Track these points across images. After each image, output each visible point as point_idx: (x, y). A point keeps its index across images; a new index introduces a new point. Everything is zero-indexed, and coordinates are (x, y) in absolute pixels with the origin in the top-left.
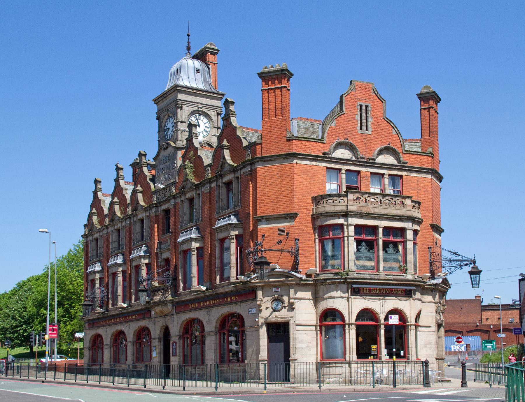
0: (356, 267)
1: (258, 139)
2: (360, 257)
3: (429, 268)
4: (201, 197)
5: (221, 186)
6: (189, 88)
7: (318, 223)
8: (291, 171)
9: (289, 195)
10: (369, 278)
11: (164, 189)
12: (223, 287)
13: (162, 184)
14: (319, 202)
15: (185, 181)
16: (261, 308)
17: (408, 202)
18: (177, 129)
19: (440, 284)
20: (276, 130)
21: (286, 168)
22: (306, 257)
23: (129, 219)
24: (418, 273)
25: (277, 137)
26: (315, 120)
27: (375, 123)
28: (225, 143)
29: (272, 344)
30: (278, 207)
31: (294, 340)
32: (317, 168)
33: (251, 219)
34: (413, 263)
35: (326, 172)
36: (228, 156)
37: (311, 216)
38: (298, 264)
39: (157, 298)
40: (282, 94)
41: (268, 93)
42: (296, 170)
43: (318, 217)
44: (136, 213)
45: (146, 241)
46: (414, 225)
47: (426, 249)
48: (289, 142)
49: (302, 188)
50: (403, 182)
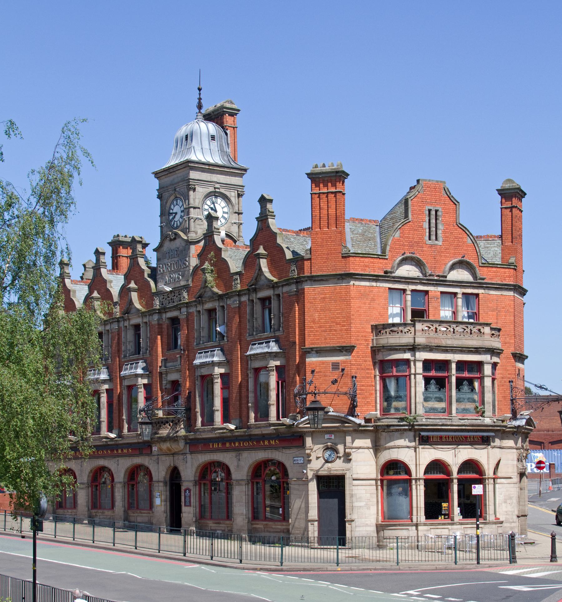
0: (424, 411)
1: (307, 254)
2: (429, 397)
3: (510, 407)
4: (225, 311)
5: (255, 302)
6: (203, 164)
7: (380, 357)
8: (347, 294)
9: (344, 323)
10: (440, 423)
11: (171, 291)
12: (259, 427)
13: (166, 284)
14: (380, 332)
15: (204, 288)
16: (310, 458)
17: (487, 330)
18: (189, 218)
19: (523, 426)
20: (328, 244)
21: (341, 291)
22: (365, 398)
23: (117, 323)
24: (496, 414)
25: (329, 252)
26: (370, 221)
27: (446, 231)
28: (261, 250)
29: (322, 500)
30: (331, 337)
31: (350, 497)
32: (378, 290)
33: (297, 349)
34: (491, 404)
35: (388, 294)
36: (265, 267)
37: (370, 349)
38: (356, 406)
39: (164, 432)
40: (336, 201)
41: (319, 197)
42: (353, 293)
43: (379, 350)
44: (128, 316)
45: (143, 356)
46: (493, 357)
47: (506, 384)
48: (345, 259)
49: (360, 315)
50: (480, 302)
